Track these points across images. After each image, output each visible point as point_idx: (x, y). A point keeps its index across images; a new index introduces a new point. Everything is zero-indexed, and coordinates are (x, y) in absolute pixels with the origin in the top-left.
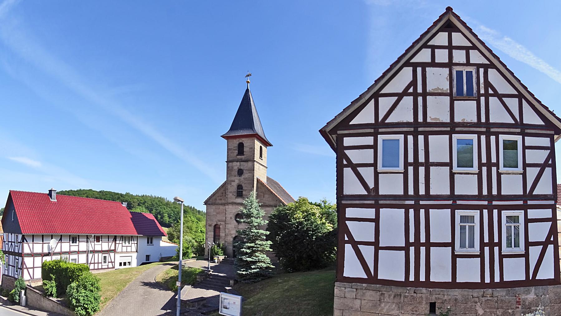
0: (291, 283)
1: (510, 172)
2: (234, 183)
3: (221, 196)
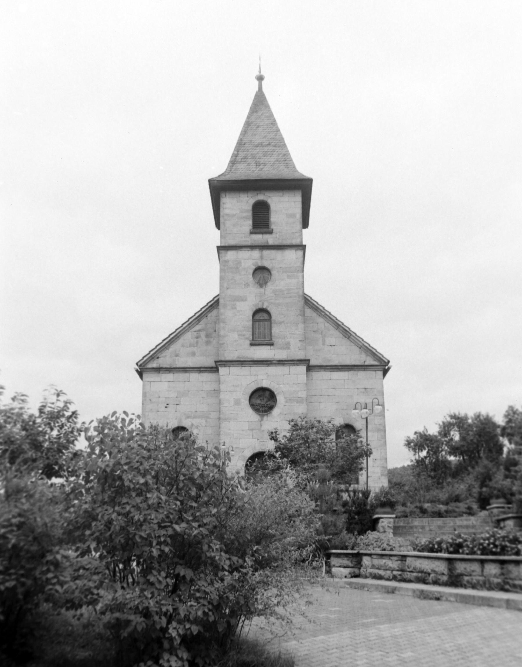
0: (388, 601)
1: (269, 333)
2: (242, 303)
3: (191, 345)
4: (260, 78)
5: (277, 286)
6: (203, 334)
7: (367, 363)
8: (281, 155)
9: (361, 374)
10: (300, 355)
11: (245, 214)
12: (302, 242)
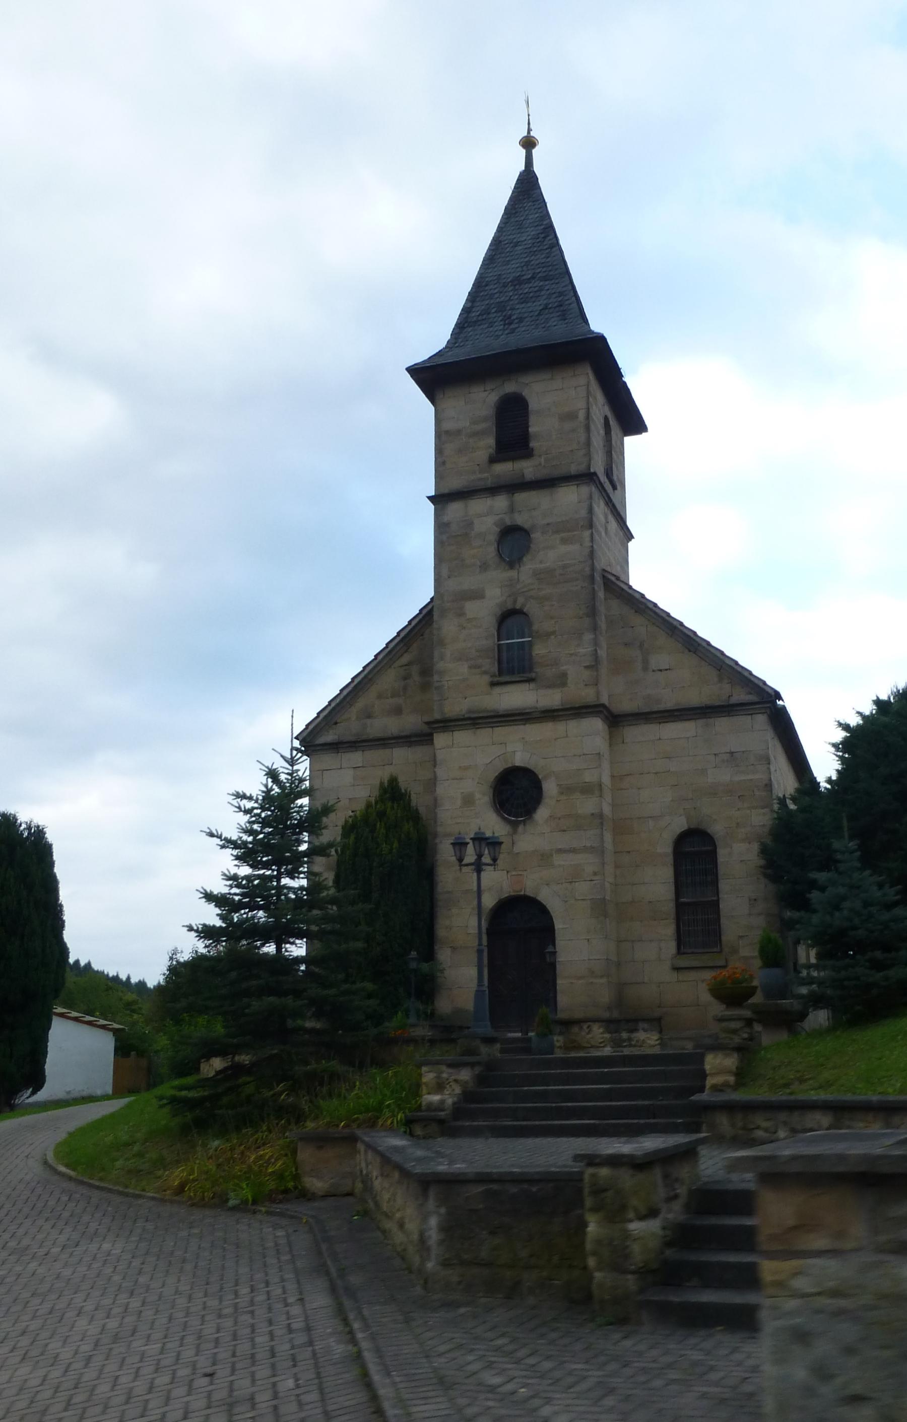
4: (529, 143)
5: (541, 562)
6: (415, 669)
7: (734, 700)
8: (554, 296)
9: (722, 724)
10: (588, 695)
11: (483, 426)
12: (589, 467)
